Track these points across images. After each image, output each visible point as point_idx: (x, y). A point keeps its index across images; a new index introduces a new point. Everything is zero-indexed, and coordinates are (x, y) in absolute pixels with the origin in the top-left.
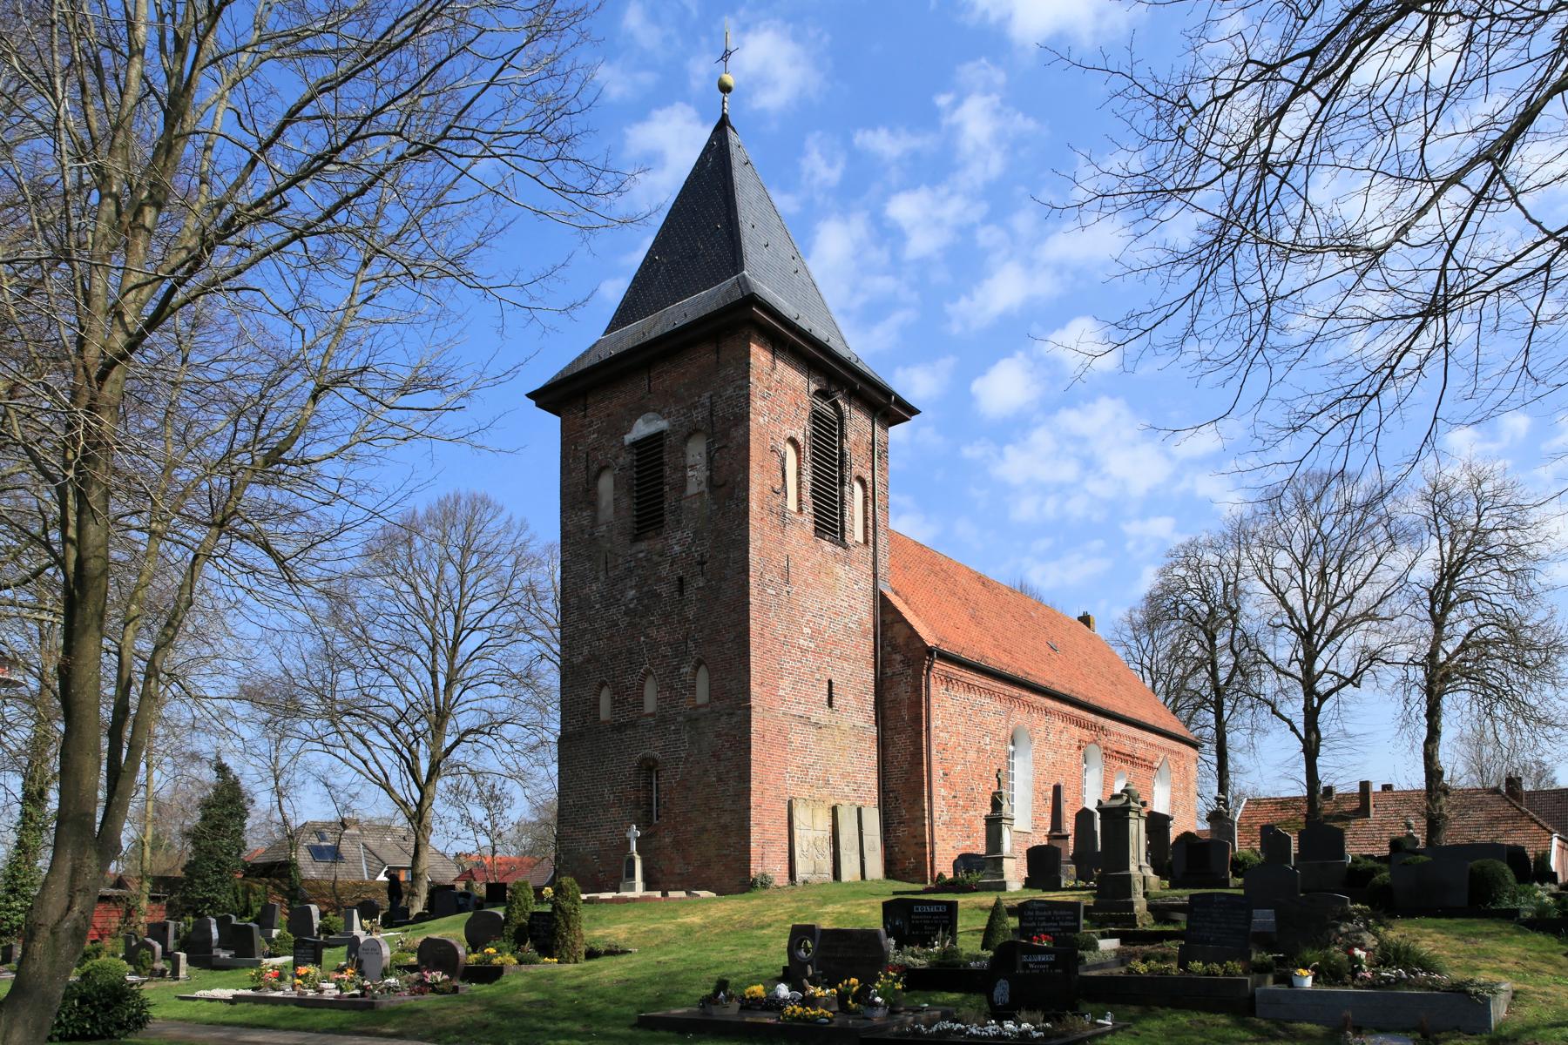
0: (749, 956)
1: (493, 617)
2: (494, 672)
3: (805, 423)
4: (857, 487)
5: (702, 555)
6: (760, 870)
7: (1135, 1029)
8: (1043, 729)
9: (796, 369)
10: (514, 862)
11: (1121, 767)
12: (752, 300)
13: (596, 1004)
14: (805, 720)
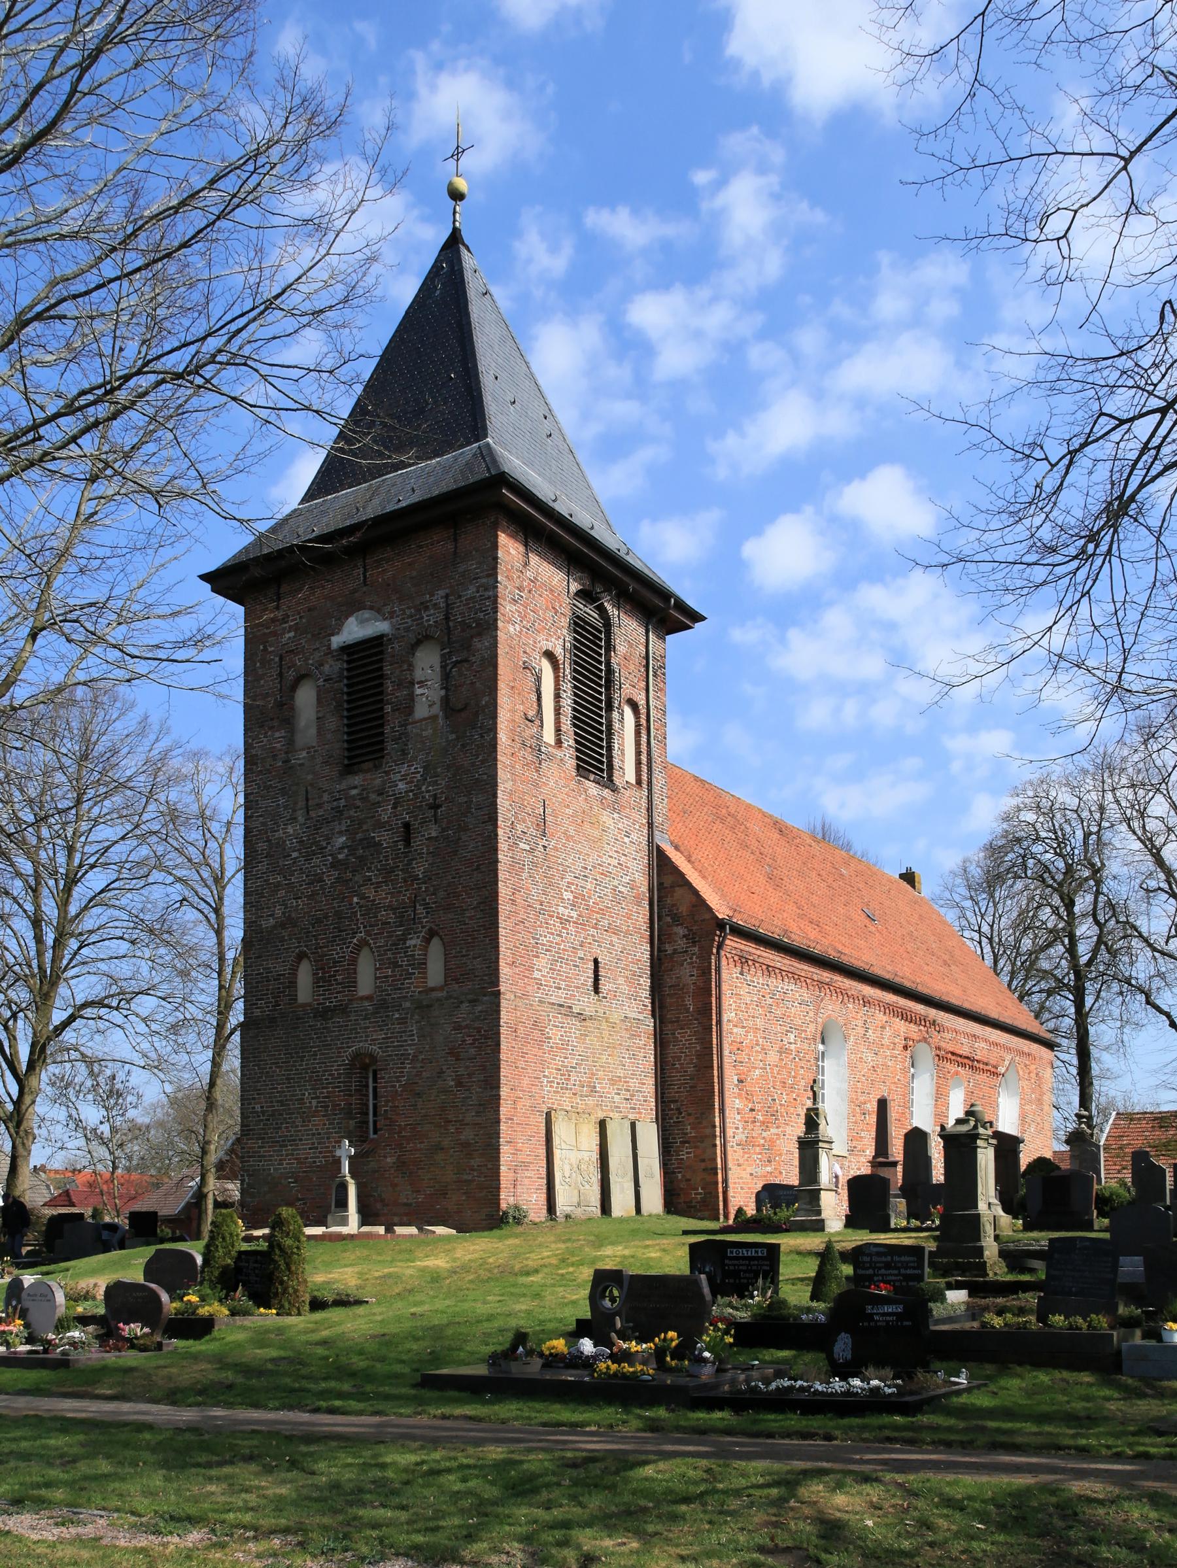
0: (524, 1307)
3: (565, 632)
4: (628, 712)
5: (435, 797)
6: (511, 1200)
7: (992, 1388)
8: (860, 1023)
9: (553, 564)
11: (957, 1073)
12: (502, 480)
13: (360, 1363)
14: (565, 1009)
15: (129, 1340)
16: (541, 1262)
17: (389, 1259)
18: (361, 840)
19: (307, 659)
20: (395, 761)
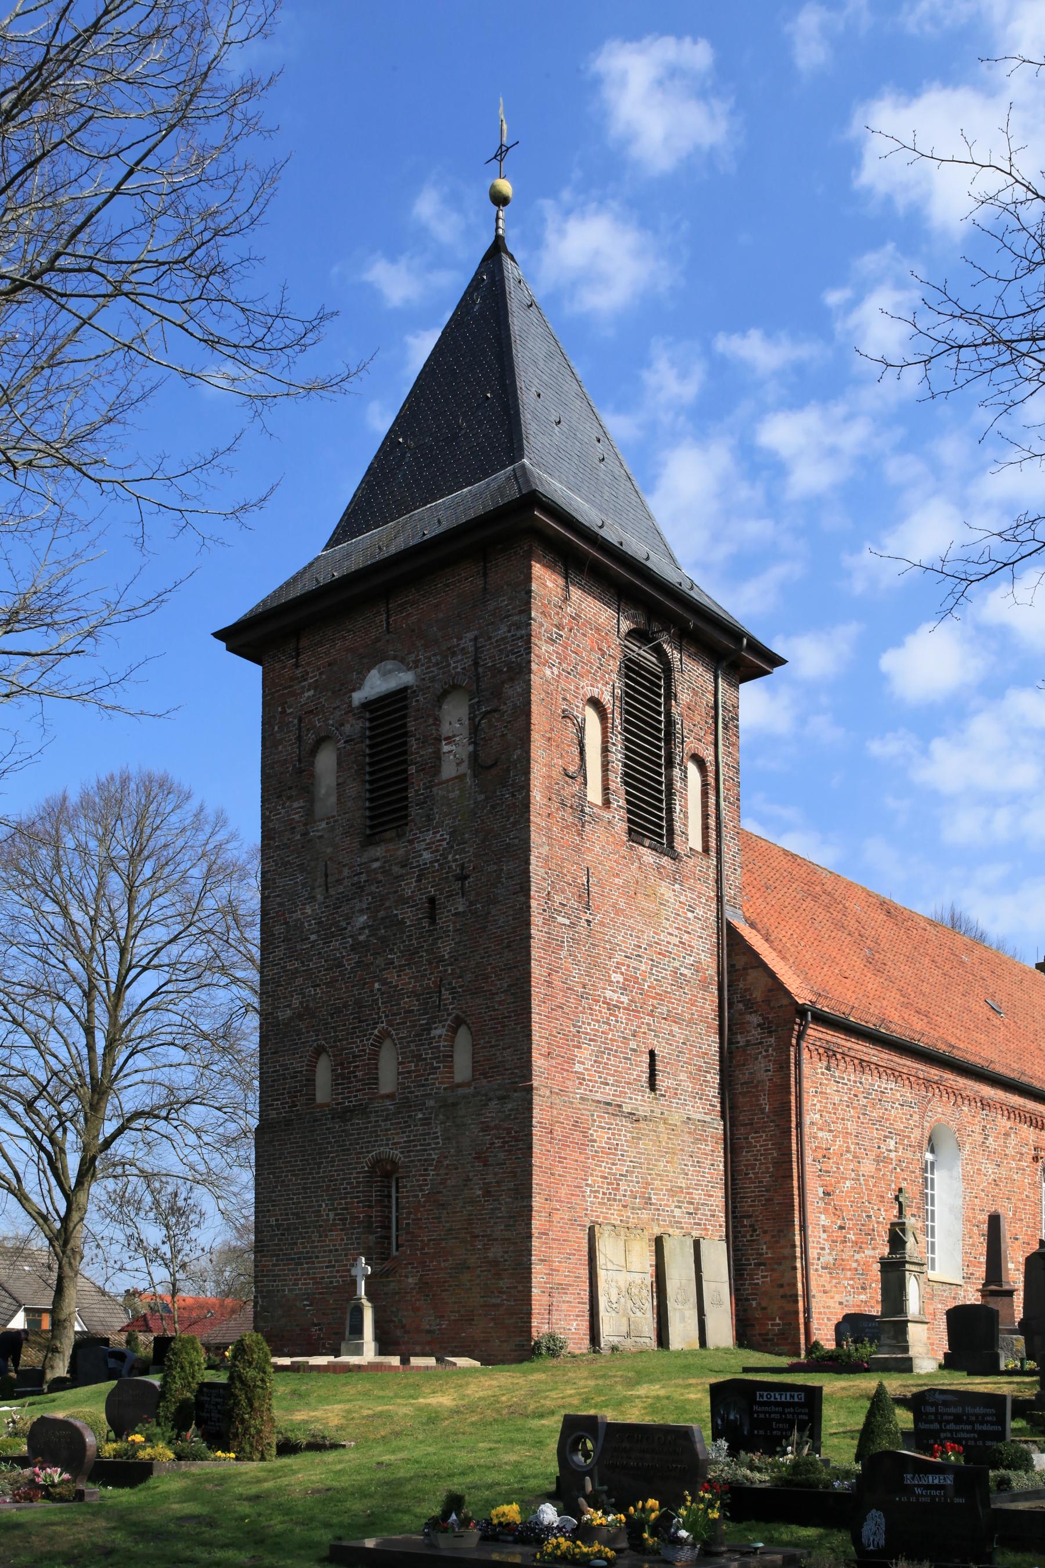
0: (513, 1457)
1: (175, 949)
2: (175, 1029)
3: (614, 676)
4: (692, 770)
5: (462, 867)
6: (545, 1329)
8: (978, 1129)
9: (600, 600)
10: (213, 1306)
13: (277, 1524)
14: (614, 1108)
15: (44, 1488)
16: (560, 1402)
17: (391, 1394)
18: (382, 919)
19: (327, 720)
20: (419, 829)
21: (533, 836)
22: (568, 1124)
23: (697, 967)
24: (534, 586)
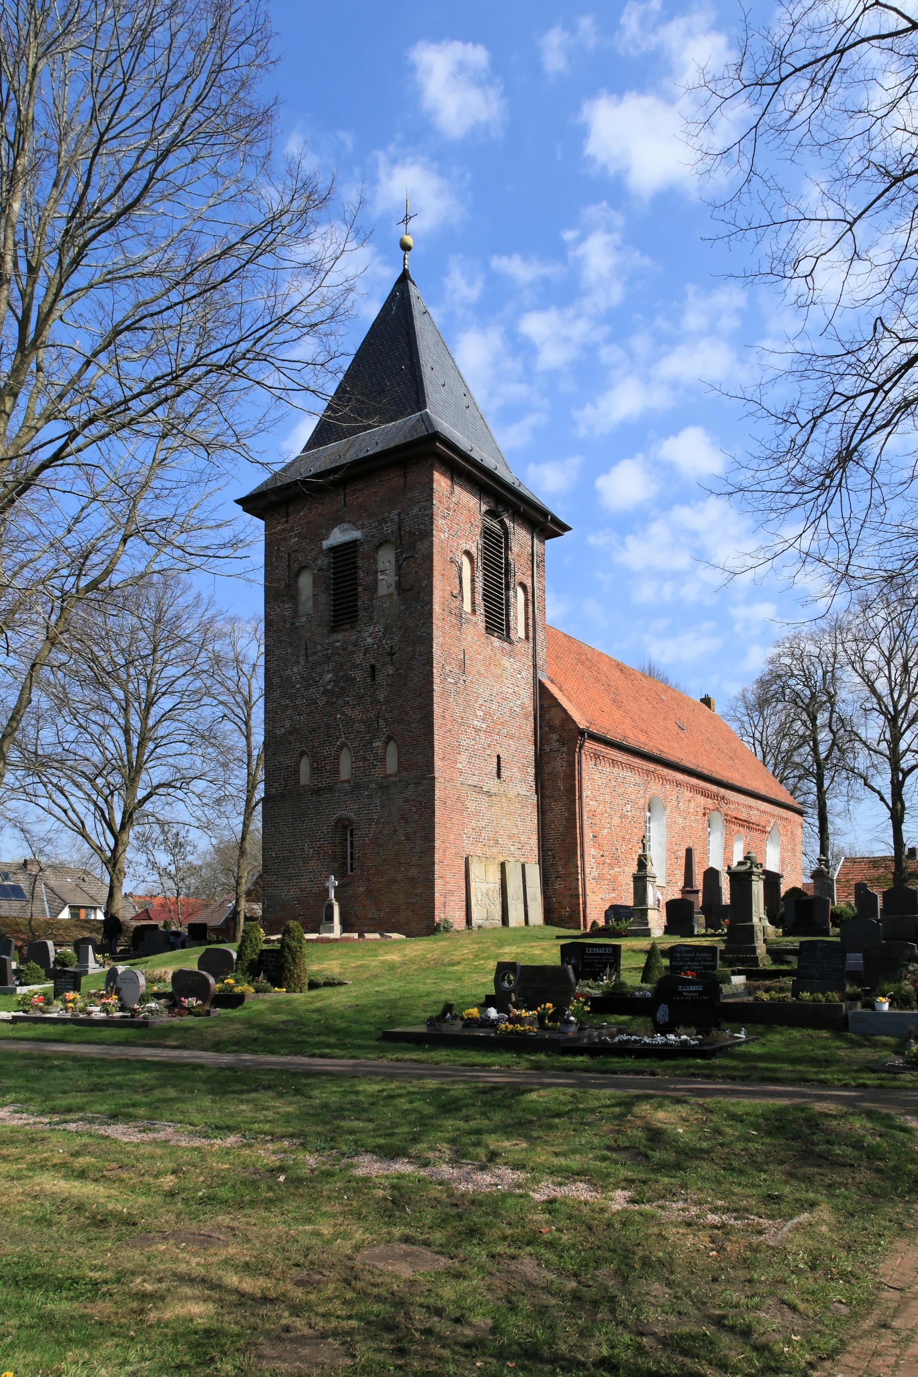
4: (520, 591)
5: (391, 648)
7: (762, 1040)
8: (674, 798)
9: (470, 493)
14: (477, 788)
21: (435, 631)
22: (454, 798)
23: (522, 706)
24: (435, 486)
